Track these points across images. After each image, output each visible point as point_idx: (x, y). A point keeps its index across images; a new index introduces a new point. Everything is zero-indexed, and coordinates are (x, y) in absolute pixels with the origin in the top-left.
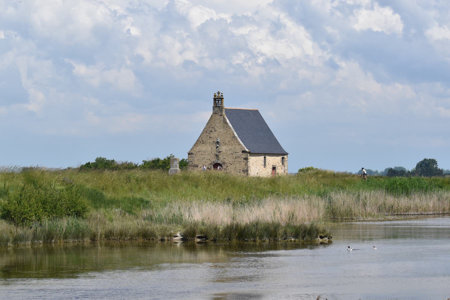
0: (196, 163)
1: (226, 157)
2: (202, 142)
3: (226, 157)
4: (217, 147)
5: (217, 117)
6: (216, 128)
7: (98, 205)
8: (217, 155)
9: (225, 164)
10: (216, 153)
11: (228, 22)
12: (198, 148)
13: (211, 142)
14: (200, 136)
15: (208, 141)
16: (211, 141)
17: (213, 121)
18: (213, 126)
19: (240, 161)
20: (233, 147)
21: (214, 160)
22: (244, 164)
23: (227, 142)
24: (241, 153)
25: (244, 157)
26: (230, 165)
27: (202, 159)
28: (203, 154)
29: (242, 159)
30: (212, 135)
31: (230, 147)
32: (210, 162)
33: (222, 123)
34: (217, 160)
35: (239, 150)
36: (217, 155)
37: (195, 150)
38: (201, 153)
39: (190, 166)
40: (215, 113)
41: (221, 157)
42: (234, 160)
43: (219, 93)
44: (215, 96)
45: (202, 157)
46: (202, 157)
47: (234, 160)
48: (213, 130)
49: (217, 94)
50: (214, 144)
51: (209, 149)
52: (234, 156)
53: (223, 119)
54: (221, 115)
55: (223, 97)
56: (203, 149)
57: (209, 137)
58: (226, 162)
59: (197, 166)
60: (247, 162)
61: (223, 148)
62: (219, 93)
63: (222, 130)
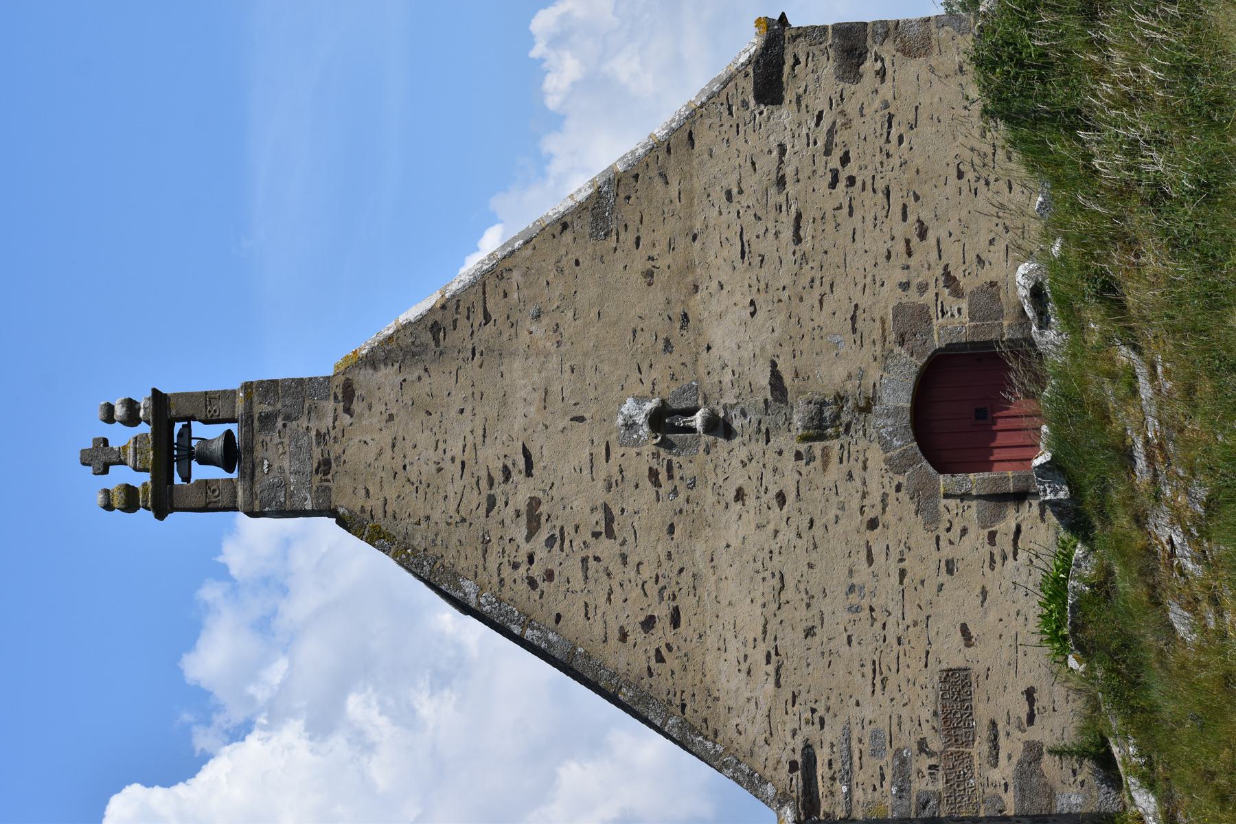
0: (920, 706)
1: (839, 301)
2: (663, 633)
3: (839, 301)
4: (719, 427)
5: (364, 442)
6: (490, 458)
7: (811, 406)
8: (817, 430)
9: (923, 314)
10: (787, 441)
11: (251, 689)
12: (727, 679)
13: (663, 511)
14: (406, 568)
15: (649, 548)
16: (642, 506)
17: (418, 506)
18: (474, 499)
19: (872, 123)
20: (718, 220)
21: (876, 457)
22: (915, 66)
23: (657, 296)
24: (785, 114)
25: (829, 68)
26: (925, 251)
27: (864, 629)
28: (800, 616)
29: (861, 91)
30: (577, 504)
31: (718, 257)
32: (902, 509)
33: (439, 380)
34: (880, 423)
35: (751, 143)
36: (817, 430)
37: (756, 731)
38: (791, 641)
39: (957, 781)
40: (318, 495)
41: (832, 373)
42: (870, 203)
43: (100, 458)
44: (131, 500)
45: (837, 617)
46: (837, 617)
47: (870, 203)
48: (522, 491)
49: (122, 476)
50: (687, 465)
51: (737, 529)
52: (818, 197)
53: (387, 375)
54: (349, 392)
55: (143, 399)
56: (749, 617)
57: (606, 548)
58: (890, 297)
59: (957, 686)
60: (888, 30)
61: (733, 347)
62: (100, 458)
63: (521, 376)
